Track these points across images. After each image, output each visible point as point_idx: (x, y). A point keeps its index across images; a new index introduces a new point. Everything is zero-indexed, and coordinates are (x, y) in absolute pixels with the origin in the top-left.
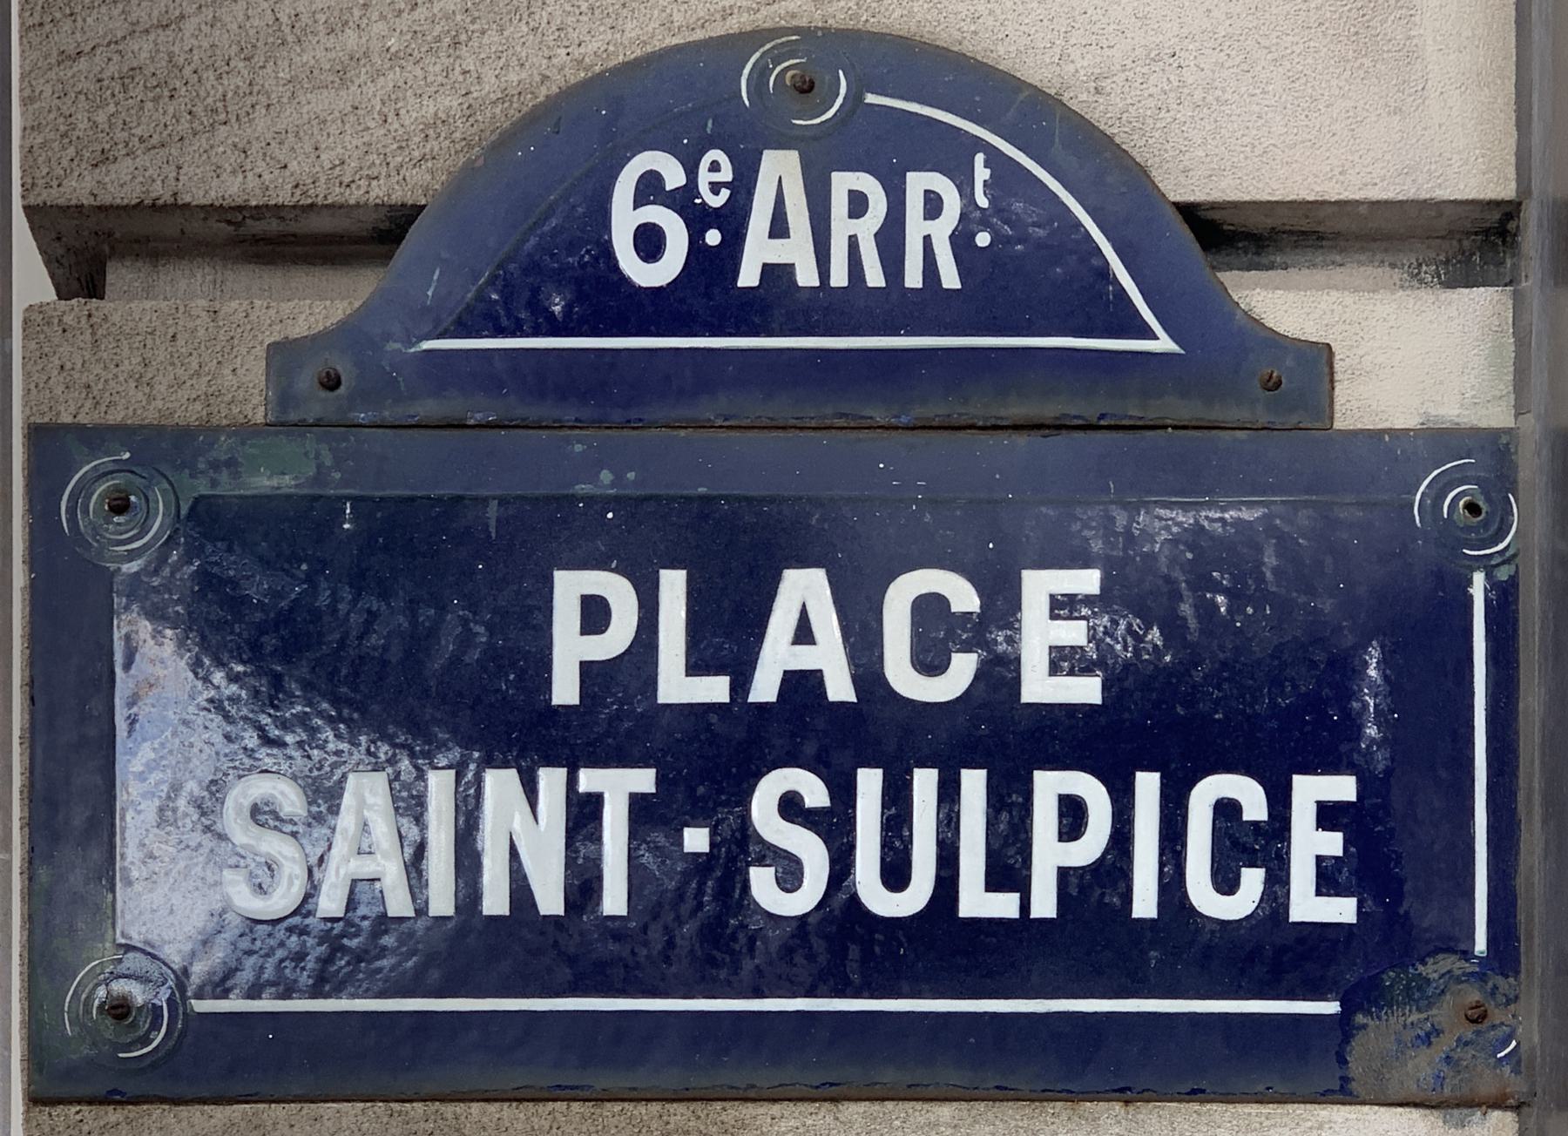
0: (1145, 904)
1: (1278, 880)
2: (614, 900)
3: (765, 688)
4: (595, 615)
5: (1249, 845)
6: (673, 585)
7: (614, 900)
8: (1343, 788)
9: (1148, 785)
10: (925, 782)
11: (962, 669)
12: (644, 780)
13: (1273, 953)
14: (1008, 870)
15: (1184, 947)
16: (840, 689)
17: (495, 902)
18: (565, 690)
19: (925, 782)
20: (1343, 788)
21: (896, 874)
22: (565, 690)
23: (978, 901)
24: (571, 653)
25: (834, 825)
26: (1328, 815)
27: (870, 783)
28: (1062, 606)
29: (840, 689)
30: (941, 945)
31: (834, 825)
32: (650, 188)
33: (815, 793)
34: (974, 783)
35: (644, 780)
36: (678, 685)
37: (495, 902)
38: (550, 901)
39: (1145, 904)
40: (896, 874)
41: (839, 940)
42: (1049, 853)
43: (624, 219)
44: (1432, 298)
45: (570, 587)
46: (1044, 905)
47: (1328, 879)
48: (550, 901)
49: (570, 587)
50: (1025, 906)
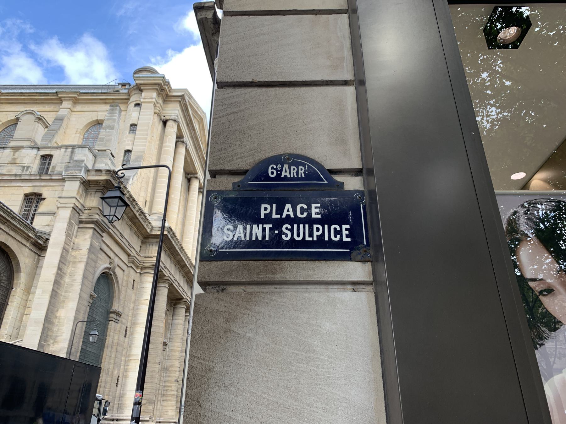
0: (326, 239)
1: (341, 236)
2: (267, 238)
7: (267, 238)
8: (348, 226)
9: (326, 226)
10: (301, 226)
12: (271, 226)
13: (341, 244)
14: (311, 235)
17: (254, 239)
19: (301, 226)
20: (348, 226)
21: (298, 235)
23: (308, 238)
24: (263, 212)
27: (295, 226)
31: (292, 230)
32: (272, 168)
33: (289, 227)
34: (307, 226)
35: (271, 226)
37: (254, 239)
38: (260, 239)
39: (326, 239)
40: (298, 235)
41: (292, 243)
42: (315, 234)
43: (270, 171)
46: (315, 239)
47: (347, 236)
48: (260, 239)
49: (263, 206)
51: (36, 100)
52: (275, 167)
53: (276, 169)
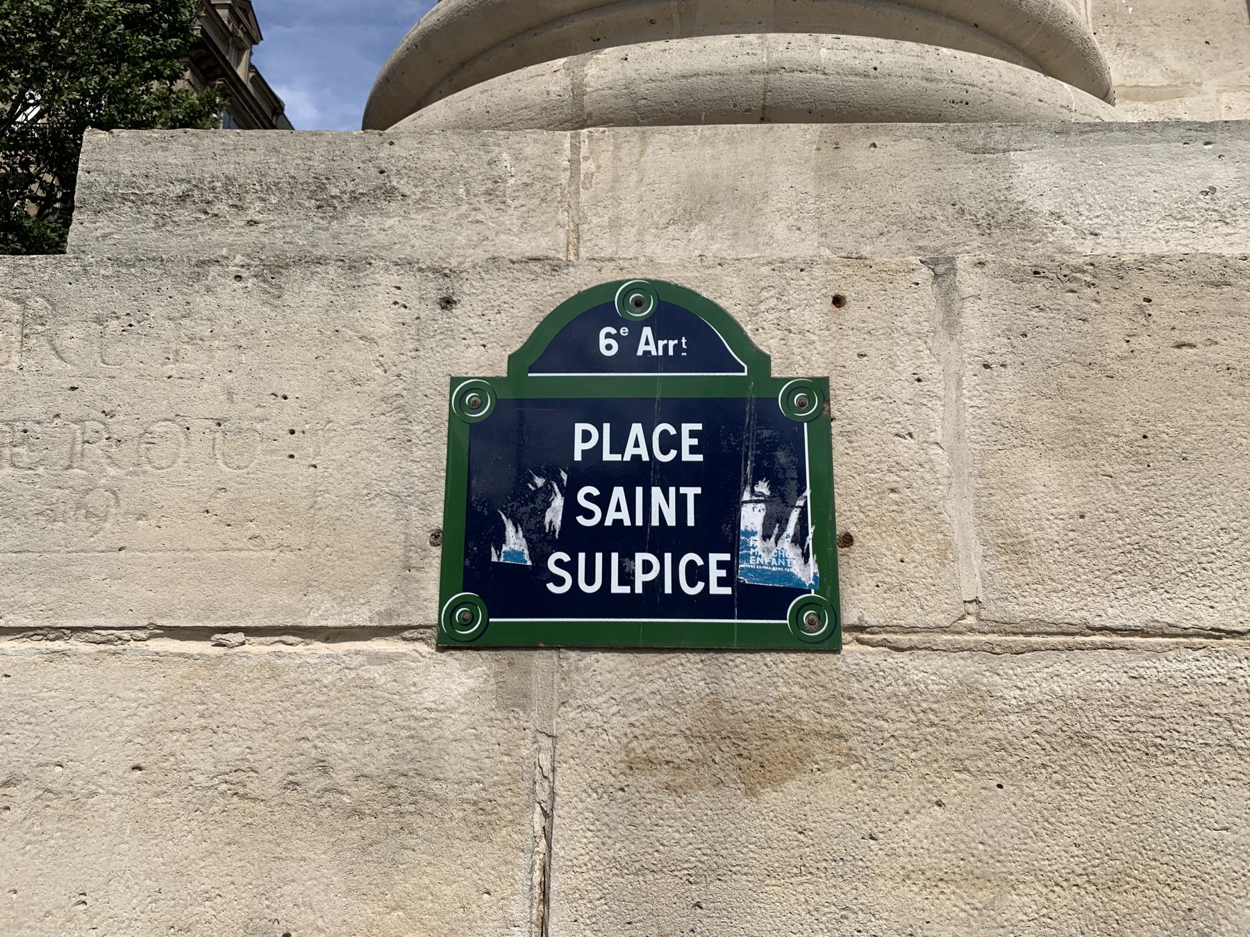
0: (668, 589)
1: (706, 580)
2: (691, 522)
3: (627, 458)
7: (691, 522)
9: (668, 557)
11: (673, 453)
12: (698, 490)
13: (706, 605)
15: (679, 604)
16: (646, 458)
17: (655, 522)
18: (578, 457)
19: (599, 557)
21: (590, 580)
22: (578, 457)
23: (616, 588)
24: (579, 447)
25: (572, 567)
27: (582, 557)
29: (646, 458)
30: (604, 602)
31: (572, 567)
32: (608, 335)
33: (566, 558)
35: (698, 490)
36: (607, 456)
37: (655, 522)
38: (671, 521)
39: (668, 589)
40: (590, 580)
41: (575, 602)
42: (640, 578)
43: (603, 342)
45: (579, 428)
46: (639, 589)
47: (721, 582)
48: (671, 521)
49: (579, 428)
50: (633, 589)
52: (613, 331)
53: (616, 337)
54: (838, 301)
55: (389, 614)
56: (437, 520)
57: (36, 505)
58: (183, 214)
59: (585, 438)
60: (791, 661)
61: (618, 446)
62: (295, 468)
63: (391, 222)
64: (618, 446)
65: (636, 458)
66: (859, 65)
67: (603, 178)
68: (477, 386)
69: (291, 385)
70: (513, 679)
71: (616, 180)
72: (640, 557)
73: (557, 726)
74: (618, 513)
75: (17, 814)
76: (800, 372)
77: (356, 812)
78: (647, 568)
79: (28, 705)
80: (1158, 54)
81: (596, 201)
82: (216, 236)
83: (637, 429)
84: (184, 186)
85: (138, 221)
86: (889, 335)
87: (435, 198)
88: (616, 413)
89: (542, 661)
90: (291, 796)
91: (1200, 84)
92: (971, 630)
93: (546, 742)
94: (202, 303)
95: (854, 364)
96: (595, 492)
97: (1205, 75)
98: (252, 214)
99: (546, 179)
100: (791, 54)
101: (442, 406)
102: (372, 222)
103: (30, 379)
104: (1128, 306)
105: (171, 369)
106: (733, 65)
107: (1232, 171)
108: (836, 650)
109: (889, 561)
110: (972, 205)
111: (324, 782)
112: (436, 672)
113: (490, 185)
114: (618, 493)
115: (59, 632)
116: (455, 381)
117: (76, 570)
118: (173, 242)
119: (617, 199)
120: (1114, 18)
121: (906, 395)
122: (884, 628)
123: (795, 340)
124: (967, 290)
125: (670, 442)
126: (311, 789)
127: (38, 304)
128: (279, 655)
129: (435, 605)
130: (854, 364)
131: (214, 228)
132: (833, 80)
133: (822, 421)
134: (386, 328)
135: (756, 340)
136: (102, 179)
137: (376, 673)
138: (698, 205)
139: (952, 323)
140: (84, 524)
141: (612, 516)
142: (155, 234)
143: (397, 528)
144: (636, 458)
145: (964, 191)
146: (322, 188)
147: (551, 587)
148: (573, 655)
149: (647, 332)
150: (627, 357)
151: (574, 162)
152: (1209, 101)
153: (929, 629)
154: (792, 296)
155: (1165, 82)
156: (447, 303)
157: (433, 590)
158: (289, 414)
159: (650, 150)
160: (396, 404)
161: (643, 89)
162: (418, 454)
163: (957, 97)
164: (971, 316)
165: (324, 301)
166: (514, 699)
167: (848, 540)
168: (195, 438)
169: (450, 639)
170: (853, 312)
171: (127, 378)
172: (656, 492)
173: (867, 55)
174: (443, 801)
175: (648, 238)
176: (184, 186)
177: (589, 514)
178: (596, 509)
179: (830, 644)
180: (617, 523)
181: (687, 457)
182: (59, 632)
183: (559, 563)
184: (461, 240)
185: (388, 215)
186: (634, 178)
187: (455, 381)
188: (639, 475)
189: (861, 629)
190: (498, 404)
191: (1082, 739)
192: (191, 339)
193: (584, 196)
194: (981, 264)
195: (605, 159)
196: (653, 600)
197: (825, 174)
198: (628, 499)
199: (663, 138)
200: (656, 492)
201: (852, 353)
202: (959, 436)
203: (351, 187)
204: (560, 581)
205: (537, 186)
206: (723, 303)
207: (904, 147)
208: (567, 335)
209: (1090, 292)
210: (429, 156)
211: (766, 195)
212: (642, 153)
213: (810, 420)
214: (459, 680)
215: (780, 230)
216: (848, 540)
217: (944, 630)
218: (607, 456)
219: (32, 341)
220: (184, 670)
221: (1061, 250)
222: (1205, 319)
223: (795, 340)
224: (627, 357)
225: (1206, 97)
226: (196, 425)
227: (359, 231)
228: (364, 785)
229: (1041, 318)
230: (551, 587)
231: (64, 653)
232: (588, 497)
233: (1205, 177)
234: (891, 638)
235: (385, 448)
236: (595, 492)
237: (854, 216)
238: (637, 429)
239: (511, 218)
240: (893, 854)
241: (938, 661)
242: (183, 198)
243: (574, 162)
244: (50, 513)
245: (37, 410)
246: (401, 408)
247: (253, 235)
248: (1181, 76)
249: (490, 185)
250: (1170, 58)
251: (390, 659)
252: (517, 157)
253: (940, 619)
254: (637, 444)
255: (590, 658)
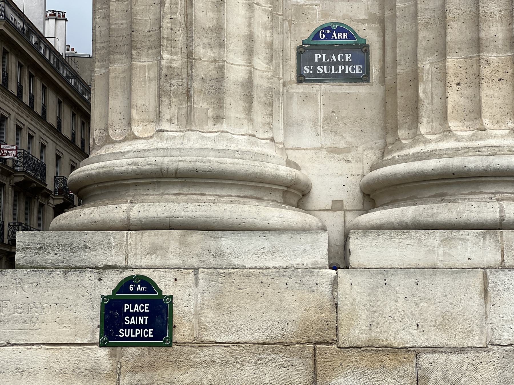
2: (146, 323)
4: (127, 307)
5: (147, 333)
6: (324, 55)
7: (146, 323)
8: (152, 330)
13: (148, 339)
14: (134, 334)
15: (143, 339)
17: (139, 323)
20: (152, 330)
21: (127, 334)
23: (132, 336)
24: (126, 309)
26: (151, 331)
28: (130, 320)
30: (130, 338)
31: (124, 332)
36: (131, 311)
37: (139, 323)
38: (142, 323)
40: (127, 334)
41: (124, 338)
42: (136, 334)
43: (130, 288)
44: (156, 264)
45: (126, 305)
48: (142, 323)
49: (126, 305)
51: (196, 182)
53: (133, 287)
54: (176, 280)
55: (90, 341)
56: (99, 323)
57: (23, 321)
58: (41, 252)
59: (127, 307)
60: (164, 349)
61: (133, 309)
62: (72, 313)
63: (87, 254)
64: (133, 309)
65: (136, 311)
66: (191, 215)
67: (134, 243)
68: (106, 297)
69: (70, 297)
70: (113, 352)
71: (136, 244)
72: (136, 330)
73: (121, 360)
74: (132, 322)
75: (25, 377)
76: (168, 294)
77: (85, 376)
78: (138, 332)
79: (25, 358)
80: (344, 135)
81: (132, 249)
82: (48, 257)
83: (136, 305)
84: (40, 245)
85: (30, 254)
86: (185, 287)
87: (96, 248)
88: (133, 302)
89: (119, 349)
90: (74, 373)
91: (357, 147)
92: (196, 343)
93: (119, 363)
94: (52, 280)
95: (178, 293)
96: (128, 318)
97: (360, 144)
98: (56, 252)
99: (121, 244)
100: (176, 213)
101: (99, 301)
102: (83, 254)
103: (19, 296)
104: (230, 281)
105: (46, 293)
106: (162, 216)
107: (268, 244)
108: (171, 346)
109: (182, 330)
110: (212, 251)
111: (79, 371)
112: (99, 351)
113: (108, 245)
114: (133, 318)
115: (31, 345)
116: (102, 296)
117: (31, 333)
118: (39, 258)
119: (136, 248)
120: (330, 121)
121: (187, 299)
122: (180, 343)
123: (167, 287)
124: (200, 278)
125: (143, 308)
126: (77, 372)
127: (18, 280)
128: (70, 348)
129: (99, 339)
130: (178, 293)
131: (48, 255)
132: (185, 219)
133: (171, 304)
134: (88, 285)
135: (160, 287)
136: (22, 243)
137: (88, 351)
138: (154, 250)
139: (197, 284)
140: (32, 324)
141: (131, 322)
142: (35, 257)
143: (91, 324)
144: (136, 311)
145: (211, 247)
146: (71, 245)
147: (120, 336)
148: (124, 348)
149: (139, 285)
150: (135, 291)
151: (127, 240)
152: (360, 154)
153: (188, 343)
154: (167, 279)
155: (346, 146)
156: (100, 280)
157: (98, 336)
158: (70, 303)
159: (144, 236)
160: (91, 301)
161: (143, 220)
162: (95, 310)
163: (214, 221)
164: (201, 282)
165: (76, 279)
166: (112, 356)
167: (175, 326)
168: (52, 307)
169: (102, 345)
170: (178, 282)
171: (38, 295)
172: (140, 318)
173: (193, 213)
174: (101, 374)
175: (143, 258)
176: (40, 245)
177: (127, 322)
178: (129, 321)
179: (170, 346)
180: (133, 324)
181: (146, 311)
182: (31, 345)
183: (121, 331)
184: (102, 258)
185: (86, 252)
186: (140, 244)
187: (102, 296)
188: (137, 314)
189: (176, 342)
190: (110, 300)
191: (213, 362)
192: (50, 287)
193: (129, 248)
194: (203, 272)
195: (134, 239)
196: (139, 338)
197: (182, 243)
198: (136, 316)
199: (147, 233)
200: (140, 318)
201: (178, 290)
202: (196, 307)
203: (78, 245)
204: (122, 335)
205: (119, 245)
206: (154, 280)
207: (199, 236)
208: (123, 286)
209: (224, 278)
210: (95, 238)
211: (168, 248)
212: (142, 238)
213: (169, 303)
214: (103, 353)
215: (171, 256)
216: (175, 326)
217: (190, 343)
218: (131, 311)
219: (18, 288)
220: (53, 351)
221: (230, 261)
222: (245, 284)
223: (167, 287)
224: (135, 291)
225: (359, 152)
226: (52, 305)
227: (80, 256)
228: (87, 371)
229: (213, 283)
230: (120, 336)
231: (30, 348)
232: (127, 319)
233: (262, 245)
234: (183, 344)
235: (88, 309)
236: (128, 318)
237: (187, 253)
238: (136, 305)
239: (113, 253)
240: (179, 381)
241: (189, 348)
242: (40, 248)
243: (127, 240)
244: (25, 322)
245: (21, 302)
246: (91, 301)
247: (56, 257)
248: (351, 144)
249: (108, 245)
250: (349, 138)
251: (91, 349)
252: (114, 238)
253: (190, 341)
254: (136, 309)
255: (127, 349)
